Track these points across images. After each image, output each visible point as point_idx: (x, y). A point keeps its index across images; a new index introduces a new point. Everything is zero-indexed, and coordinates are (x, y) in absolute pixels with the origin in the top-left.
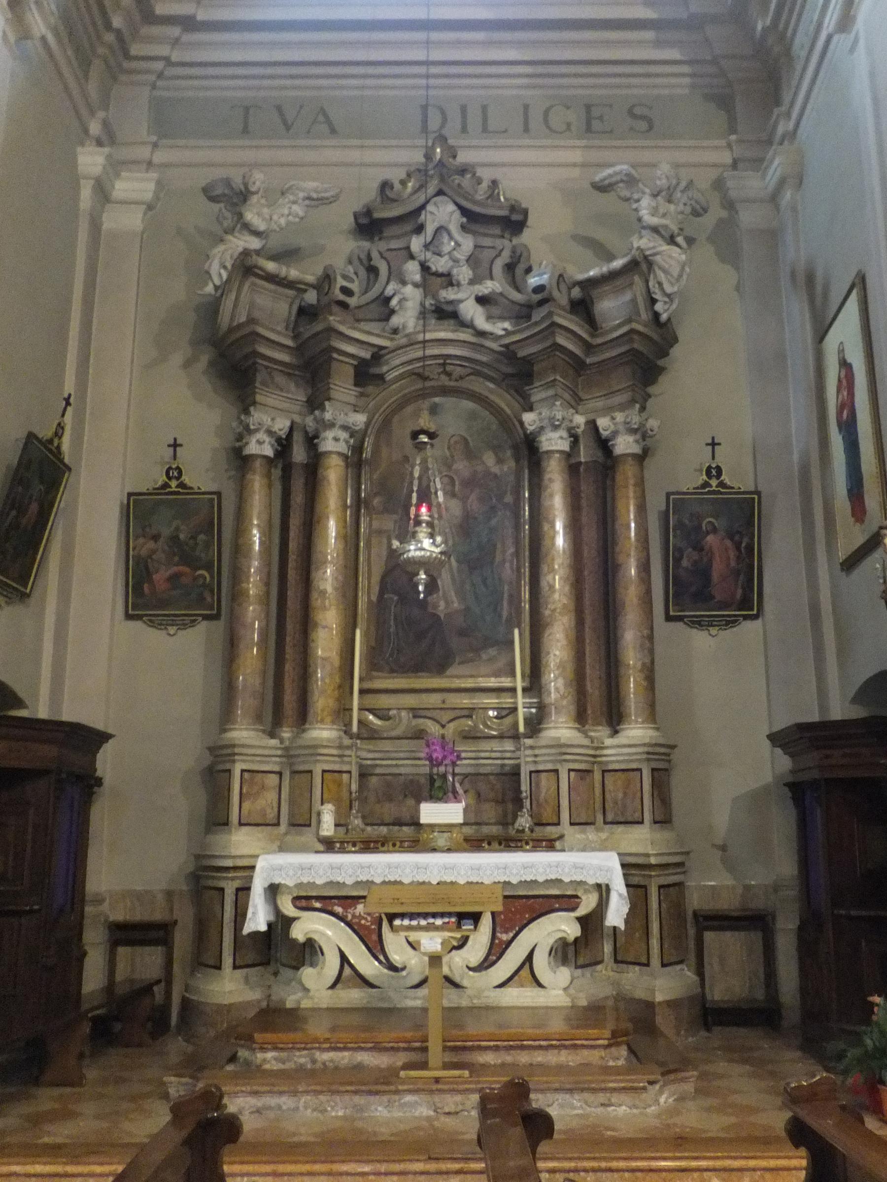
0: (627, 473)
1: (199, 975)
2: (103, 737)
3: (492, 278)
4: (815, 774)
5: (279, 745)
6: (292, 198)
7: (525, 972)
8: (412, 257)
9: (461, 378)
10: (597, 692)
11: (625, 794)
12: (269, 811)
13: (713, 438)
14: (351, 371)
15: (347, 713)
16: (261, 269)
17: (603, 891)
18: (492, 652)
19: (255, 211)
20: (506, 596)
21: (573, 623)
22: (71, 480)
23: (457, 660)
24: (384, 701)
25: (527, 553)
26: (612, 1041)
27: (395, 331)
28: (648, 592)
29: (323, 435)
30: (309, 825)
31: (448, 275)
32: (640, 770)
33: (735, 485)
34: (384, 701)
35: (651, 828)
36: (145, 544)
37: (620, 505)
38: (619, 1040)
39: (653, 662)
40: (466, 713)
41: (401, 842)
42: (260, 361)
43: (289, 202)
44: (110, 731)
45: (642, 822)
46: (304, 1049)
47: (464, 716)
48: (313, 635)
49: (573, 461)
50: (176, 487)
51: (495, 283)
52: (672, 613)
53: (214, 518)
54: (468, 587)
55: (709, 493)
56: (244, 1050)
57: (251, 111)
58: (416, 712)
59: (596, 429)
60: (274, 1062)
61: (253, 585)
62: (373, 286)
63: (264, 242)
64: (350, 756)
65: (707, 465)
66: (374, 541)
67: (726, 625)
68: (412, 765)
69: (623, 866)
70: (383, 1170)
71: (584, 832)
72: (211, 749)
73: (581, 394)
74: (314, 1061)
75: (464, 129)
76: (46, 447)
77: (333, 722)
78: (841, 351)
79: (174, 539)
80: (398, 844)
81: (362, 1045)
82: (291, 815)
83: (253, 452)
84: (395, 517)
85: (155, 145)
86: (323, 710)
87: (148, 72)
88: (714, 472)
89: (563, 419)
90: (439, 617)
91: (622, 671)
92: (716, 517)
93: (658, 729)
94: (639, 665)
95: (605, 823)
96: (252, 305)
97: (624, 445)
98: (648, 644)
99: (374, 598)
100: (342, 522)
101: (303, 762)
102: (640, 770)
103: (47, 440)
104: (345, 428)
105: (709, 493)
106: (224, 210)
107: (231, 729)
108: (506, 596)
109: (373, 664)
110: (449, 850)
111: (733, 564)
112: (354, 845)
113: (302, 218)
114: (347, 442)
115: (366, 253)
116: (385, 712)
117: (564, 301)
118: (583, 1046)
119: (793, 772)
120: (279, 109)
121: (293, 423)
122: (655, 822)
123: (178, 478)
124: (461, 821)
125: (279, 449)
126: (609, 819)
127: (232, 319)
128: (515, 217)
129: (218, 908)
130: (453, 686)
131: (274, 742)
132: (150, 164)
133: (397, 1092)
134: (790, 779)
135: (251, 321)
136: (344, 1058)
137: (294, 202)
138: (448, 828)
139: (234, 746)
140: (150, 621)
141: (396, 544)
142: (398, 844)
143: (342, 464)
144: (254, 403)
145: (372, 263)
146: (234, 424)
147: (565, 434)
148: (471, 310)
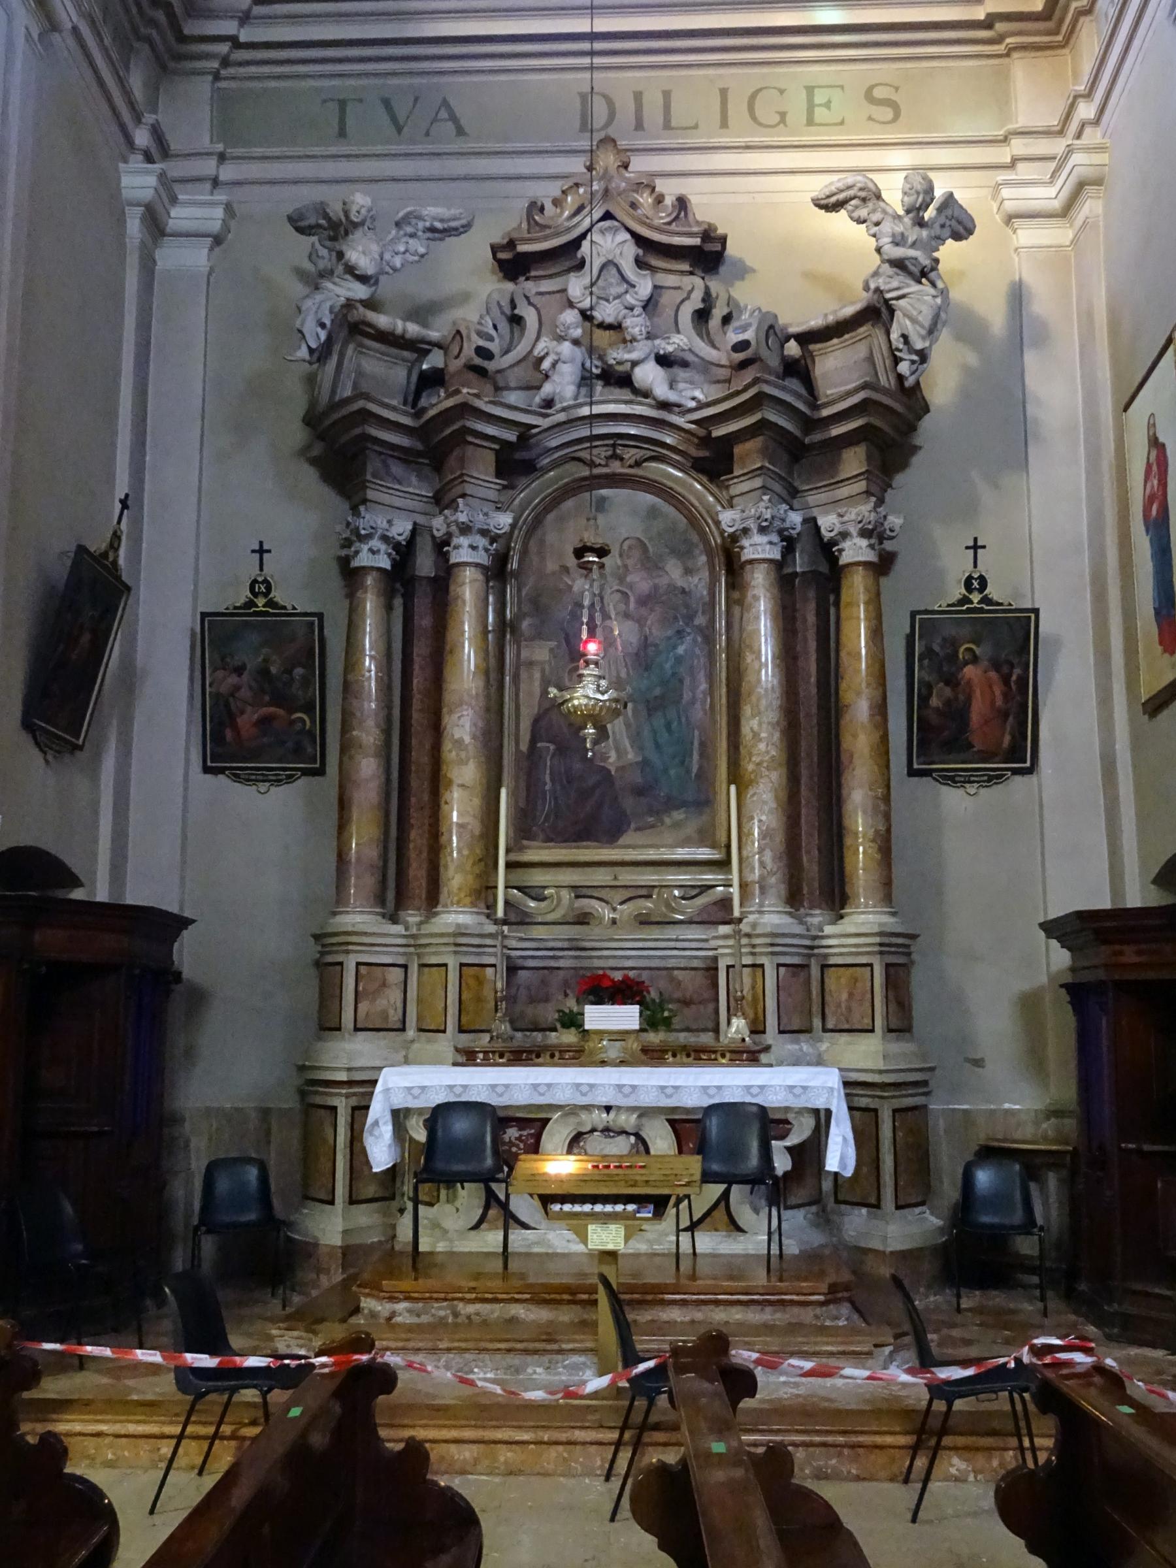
0: (856, 587)
1: (306, 1211)
2: (183, 923)
3: (678, 332)
4: (1101, 974)
5: (404, 932)
6: (409, 230)
7: (720, 1213)
8: (571, 305)
9: (638, 464)
10: (815, 868)
11: (851, 995)
12: (391, 1012)
14: (491, 457)
15: (490, 891)
16: (370, 325)
17: (822, 1119)
18: (678, 815)
19: (360, 248)
20: (696, 743)
21: (784, 781)
22: (129, 602)
23: (633, 826)
24: (537, 878)
25: (724, 690)
26: (829, 1297)
27: (549, 403)
28: (884, 738)
29: (455, 541)
30: (444, 1031)
31: (617, 327)
32: (871, 965)
34: (537, 878)
35: (884, 1038)
36: (225, 678)
37: (846, 627)
38: (840, 1295)
39: (888, 831)
40: (644, 892)
41: (560, 1052)
42: (369, 445)
43: (405, 235)
44: (187, 914)
45: (872, 1031)
46: (445, 1300)
47: (641, 897)
48: (446, 796)
49: (788, 570)
50: (979, 603)
51: (682, 337)
52: (916, 766)
53: (314, 648)
54: (646, 733)
55: (969, 611)
56: (368, 1300)
57: (349, 108)
58: (579, 892)
59: (817, 529)
60: (407, 1315)
61: (368, 734)
62: (519, 342)
63: (373, 289)
64: (495, 946)
65: (967, 575)
66: (524, 675)
67: (989, 781)
68: (576, 957)
69: (846, 1084)
70: (546, 1439)
71: (797, 1042)
72: (317, 937)
73: (796, 484)
74: (456, 1315)
75: (639, 126)
76: (99, 563)
77: (473, 905)
78: (1152, 425)
79: (264, 672)
81: (516, 1296)
82: (420, 1018)
83: (364, 563)
84: (553, 644)
85: (222, 157)
86: (460, 889)
87: (208, 56)
88: (976, 584)
89: (773, 517)
90: (609, 771)
91: (848, 841)
92: (977, 642)
93: (894, 914)
94: (871, 833)
95: (825, 1030)
96: (360, 373)
97: (855, 550)
98: (882, 807)
99: (524, 747)
100: (483, 652)
101: (435, 953)
102: (871, 965)
103: (101, 555)
104: (484, 533)
106: (317, 245)
107: (341, 913)
108: (696, 743)
109: (523, 831)
110: (623, 1063)
111: (999, 702)
112: (501, 1056)
113: (422, 256)
114: (487, 550)
115: (508, 300)
116: (539, 891)
117: (774, 362)
118: (792, 1302)
119: (1073, 970)
120: (387, 103)
121: (415, 524)
122: (890, 1031)
123: (266, 595)
124: (637, 1027)
125: (398, 558)
126: (830, 1025)
127: (333, 392)
128: (710, 247)
129: (330, 1132)
130: (627, 858)
131: (399, 929)
132: (215, 182)
133: (560, 1352)
134: (1068, 978)
135: (360, 395)
136: (494, 1311)
137: (412, 236)
138: (622, 1035)
140: (236, 775)
141: (553, 692)
142: (557, 1054)
143: (480, 577)
144: (365, 501)
145: (516, 312)
146: (338, 528)
147: (775, 538)
148: (649, 375)
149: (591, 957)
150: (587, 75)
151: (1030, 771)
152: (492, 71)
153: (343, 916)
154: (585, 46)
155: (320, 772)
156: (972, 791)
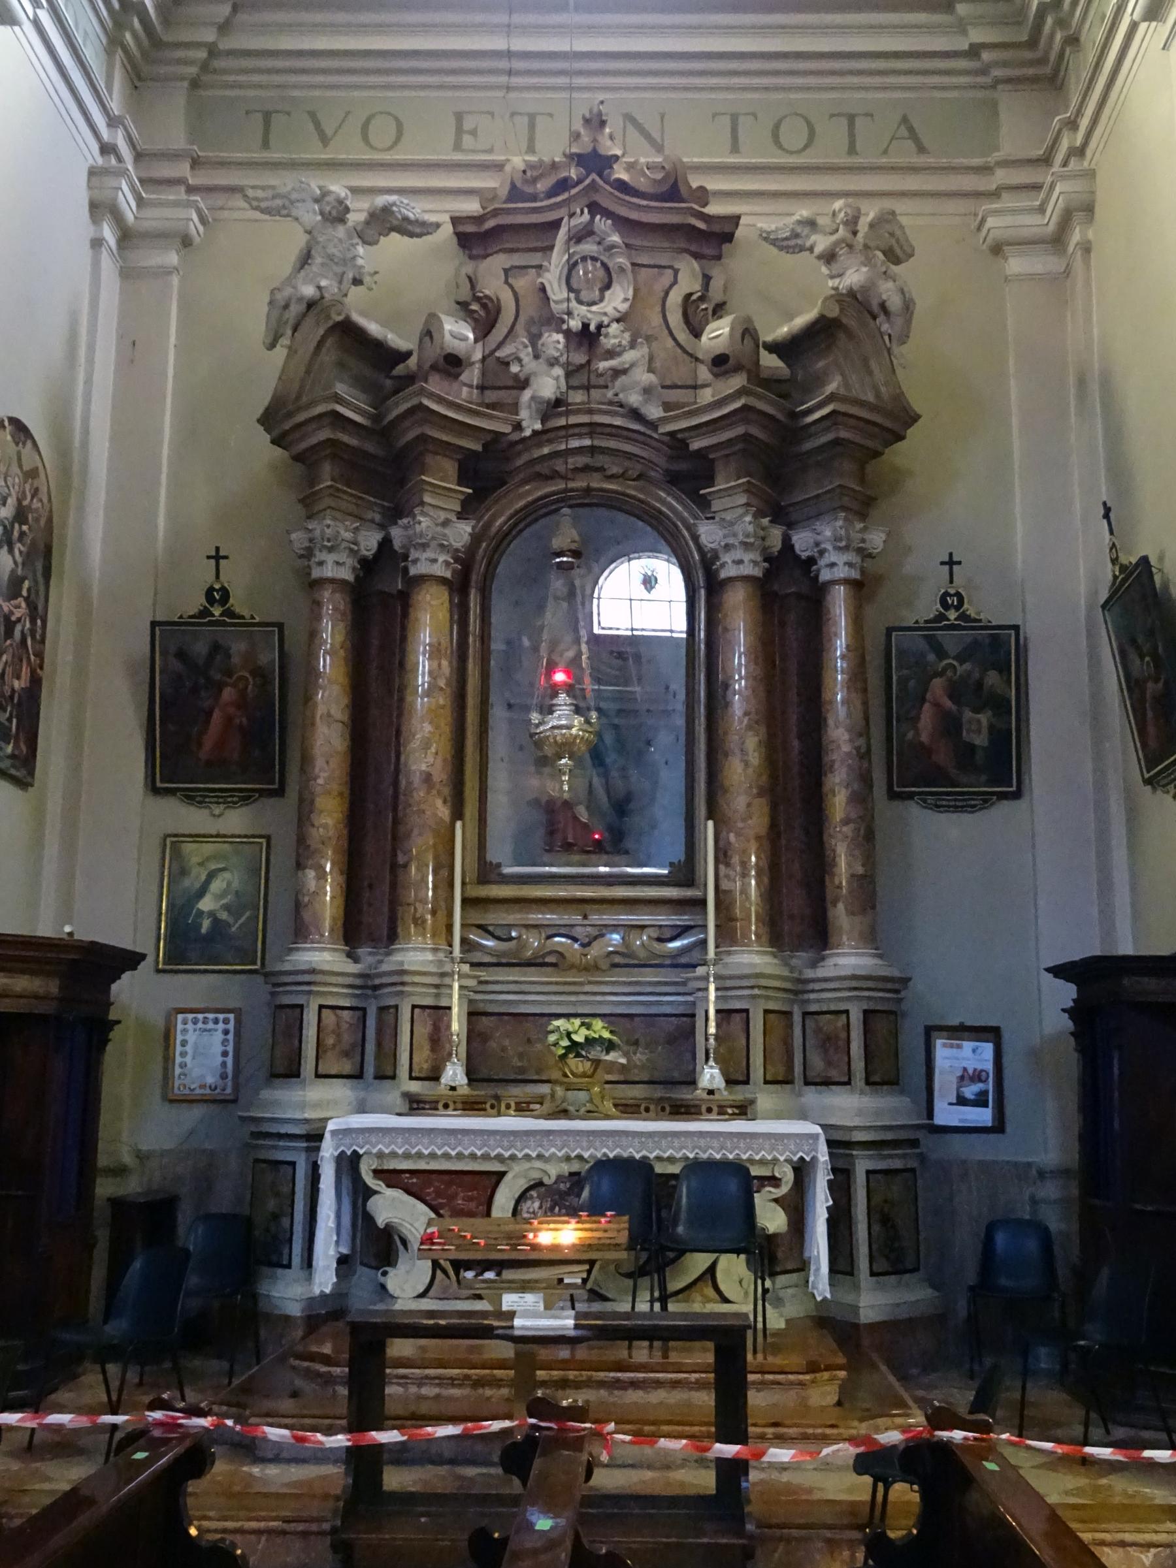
13: (951, 555)
17: (802, 1170)
33: (246, 613)
41: (455, 1102)
50: (221, 615)
55: (210, 623)
80: (715, 1109)
82: (378, 1067)
85: (196, 163)
105: (210, 623)
107: (298, 949)
123: (957, 608)
139: (403, 972)
140: (188, 797)
149: (291, 992)
150: (564, 95)
151: (1017, 795)
152: (474, 87)
153: (301, 953)
154: (503, 64)
155: (280, 792)
156: (217, 812)
